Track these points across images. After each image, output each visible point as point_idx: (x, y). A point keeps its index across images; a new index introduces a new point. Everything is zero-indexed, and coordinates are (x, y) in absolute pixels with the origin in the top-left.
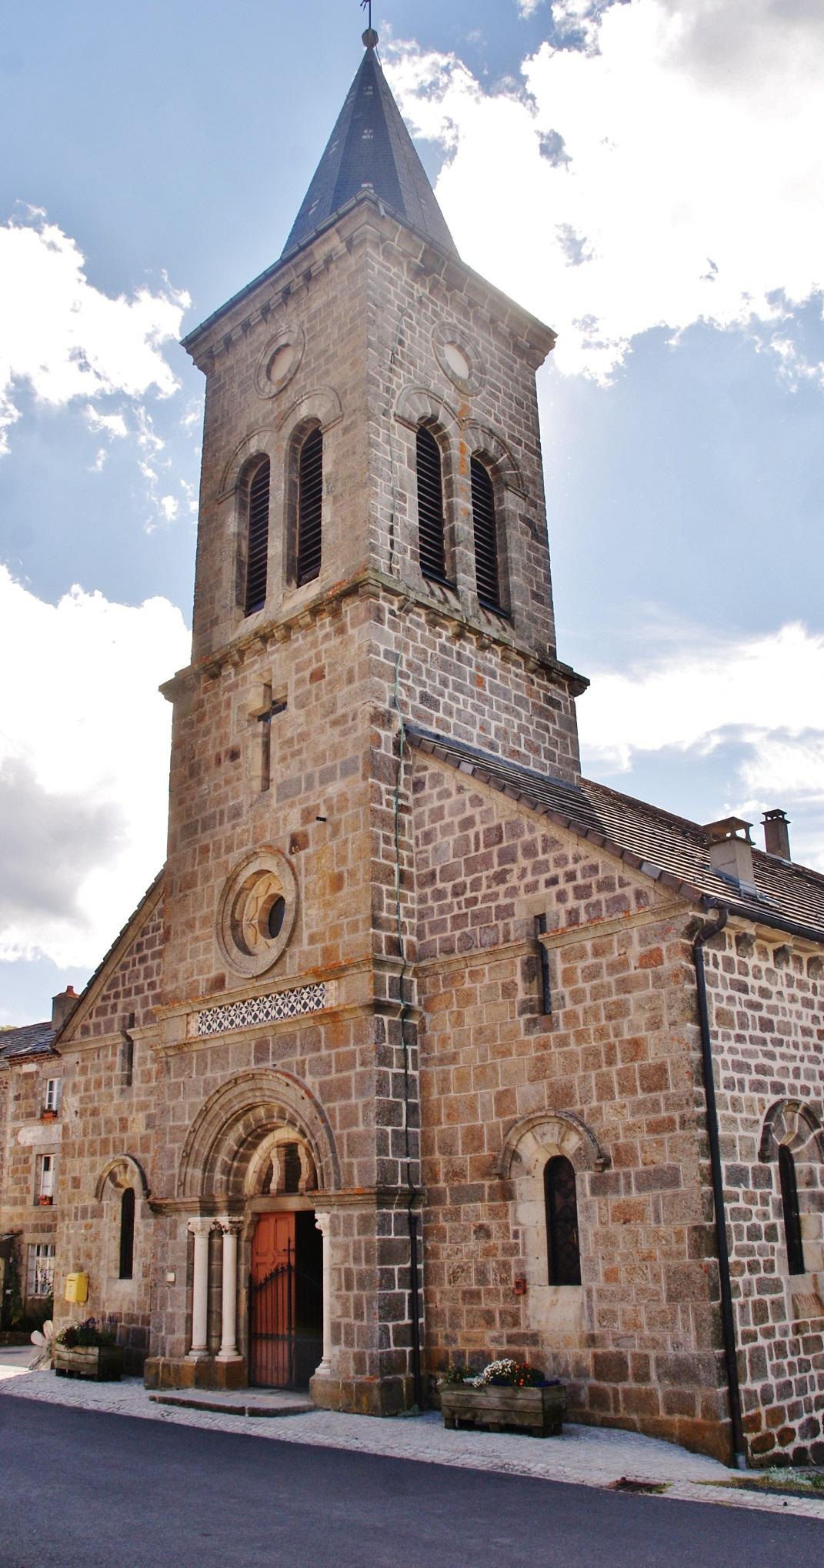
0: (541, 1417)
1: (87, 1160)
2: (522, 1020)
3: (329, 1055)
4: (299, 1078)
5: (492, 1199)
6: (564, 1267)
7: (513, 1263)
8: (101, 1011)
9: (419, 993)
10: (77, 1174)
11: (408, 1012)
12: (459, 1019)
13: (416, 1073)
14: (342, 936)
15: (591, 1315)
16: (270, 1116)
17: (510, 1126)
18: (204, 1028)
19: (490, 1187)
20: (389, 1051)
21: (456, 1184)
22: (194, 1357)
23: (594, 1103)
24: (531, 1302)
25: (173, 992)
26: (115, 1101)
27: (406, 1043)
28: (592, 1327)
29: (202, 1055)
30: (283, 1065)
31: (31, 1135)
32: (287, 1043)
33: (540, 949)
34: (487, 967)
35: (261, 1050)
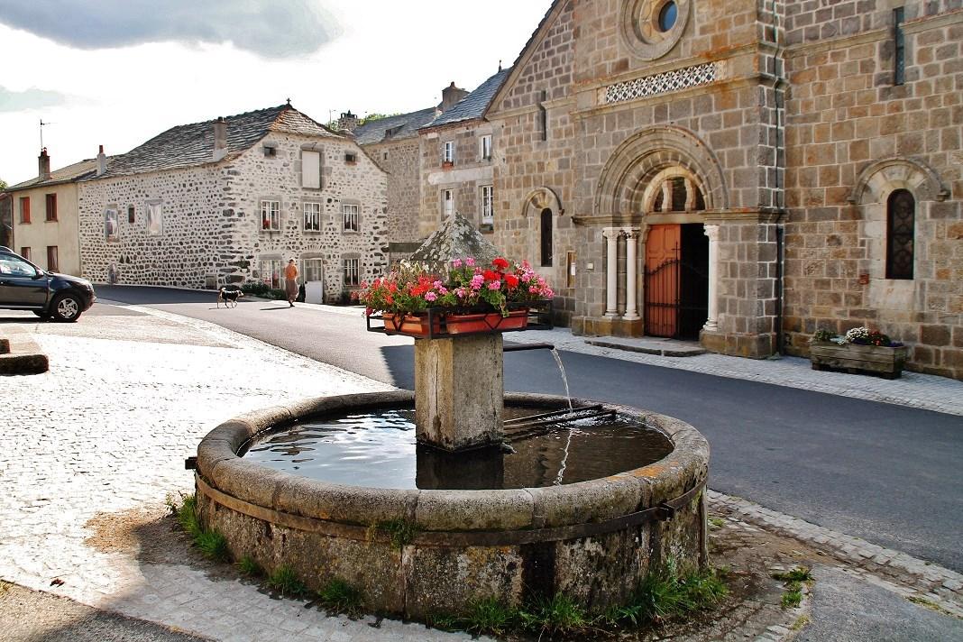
0: (892, 367)
1: (514, 191)
2: (878, 90)
3: (719, 115)
4: (693, 131)
5: (844, 218)
6: (899, 266)
7: (859, 263)
8: (519, 91)
9: (786, 70)
10: (507, 200)
11: (779, 83)
12: (821, 89)
13: (783, 128)
14: (730, 28)
15: (922, 300)
16: (665, 158)
17: (861, 169)
18: (611, 98)
19: (843, 210)
20: (767, 111)
21: (814, 207)
22: (609, 317)
23: (940, 152)
24: (872, 289)
25: (583, 73)
26: (534, 151)
27: (777, 107)
28: (923, 309)
29: (611, 118)
30: (679, 122)
31: (437, 177)
32: (683, 107)
33: (896, 33)
34: (848, 50)
35: (661, 112)
